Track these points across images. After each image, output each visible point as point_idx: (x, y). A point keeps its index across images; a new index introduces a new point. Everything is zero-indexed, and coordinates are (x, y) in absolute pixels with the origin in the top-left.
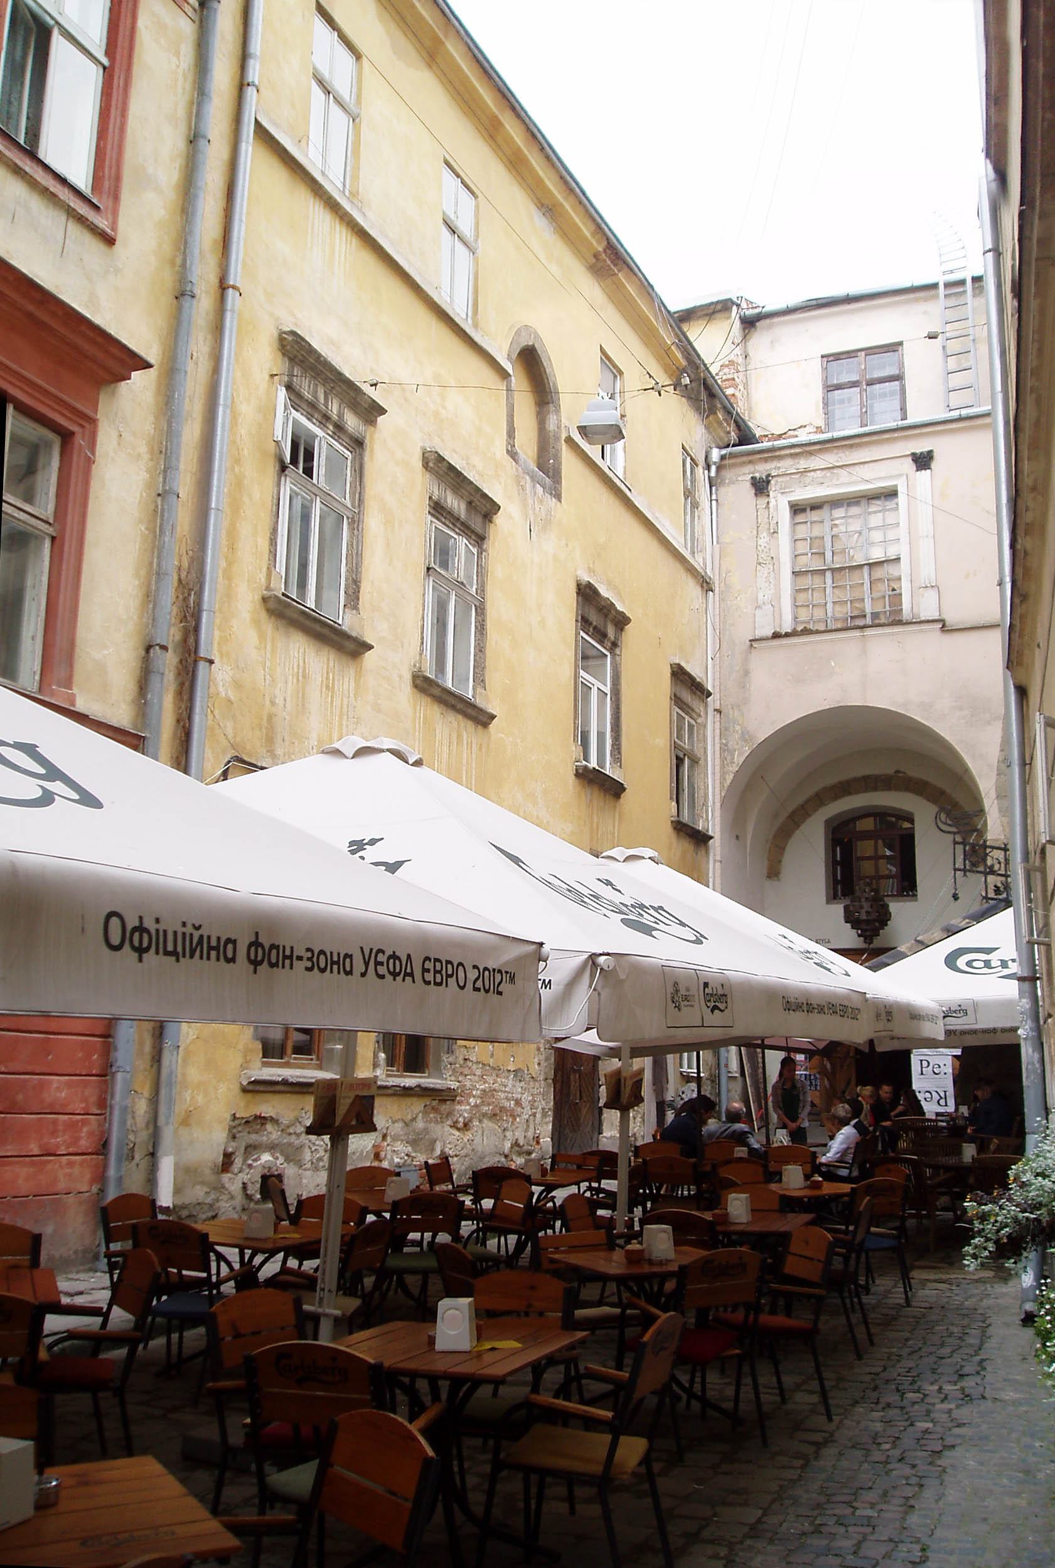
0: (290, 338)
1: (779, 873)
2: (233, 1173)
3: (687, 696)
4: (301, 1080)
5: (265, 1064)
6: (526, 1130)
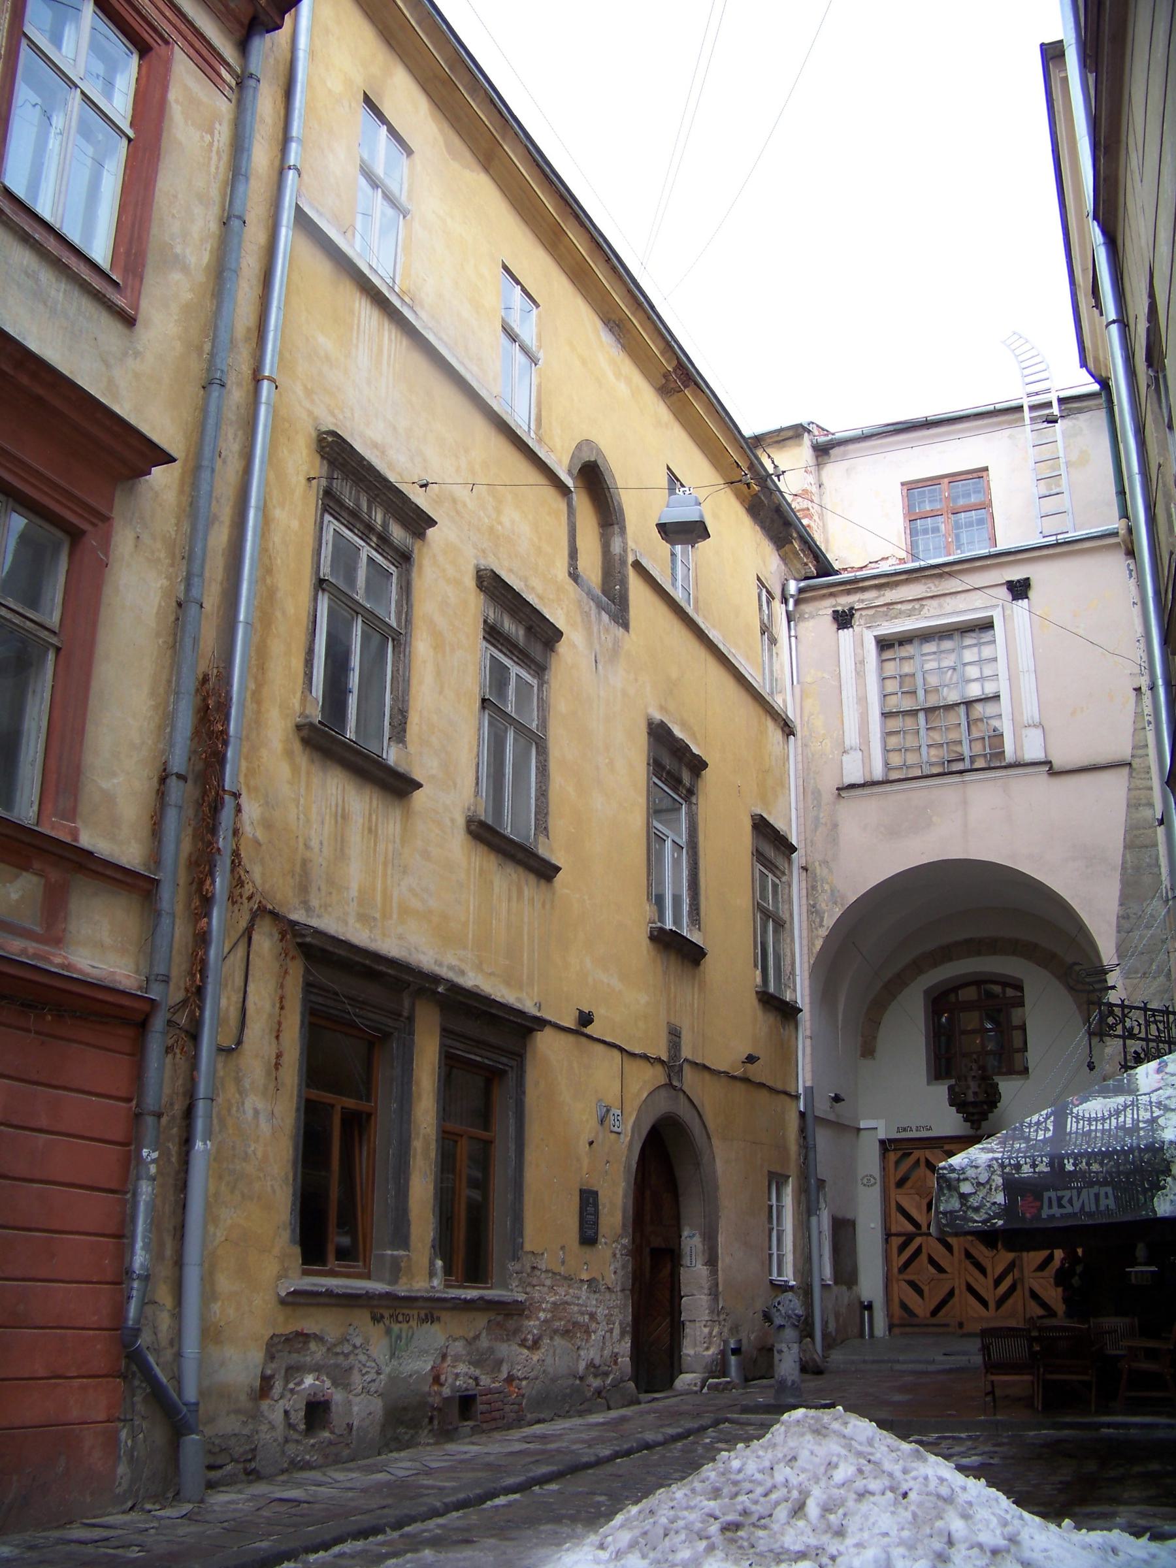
0: (330, 439)
1: (874, 1051)
2: (273, 1399)
3: (770, 852)
4: (349, 1291)
5: (305, 1273)
6: (602, 1349)
